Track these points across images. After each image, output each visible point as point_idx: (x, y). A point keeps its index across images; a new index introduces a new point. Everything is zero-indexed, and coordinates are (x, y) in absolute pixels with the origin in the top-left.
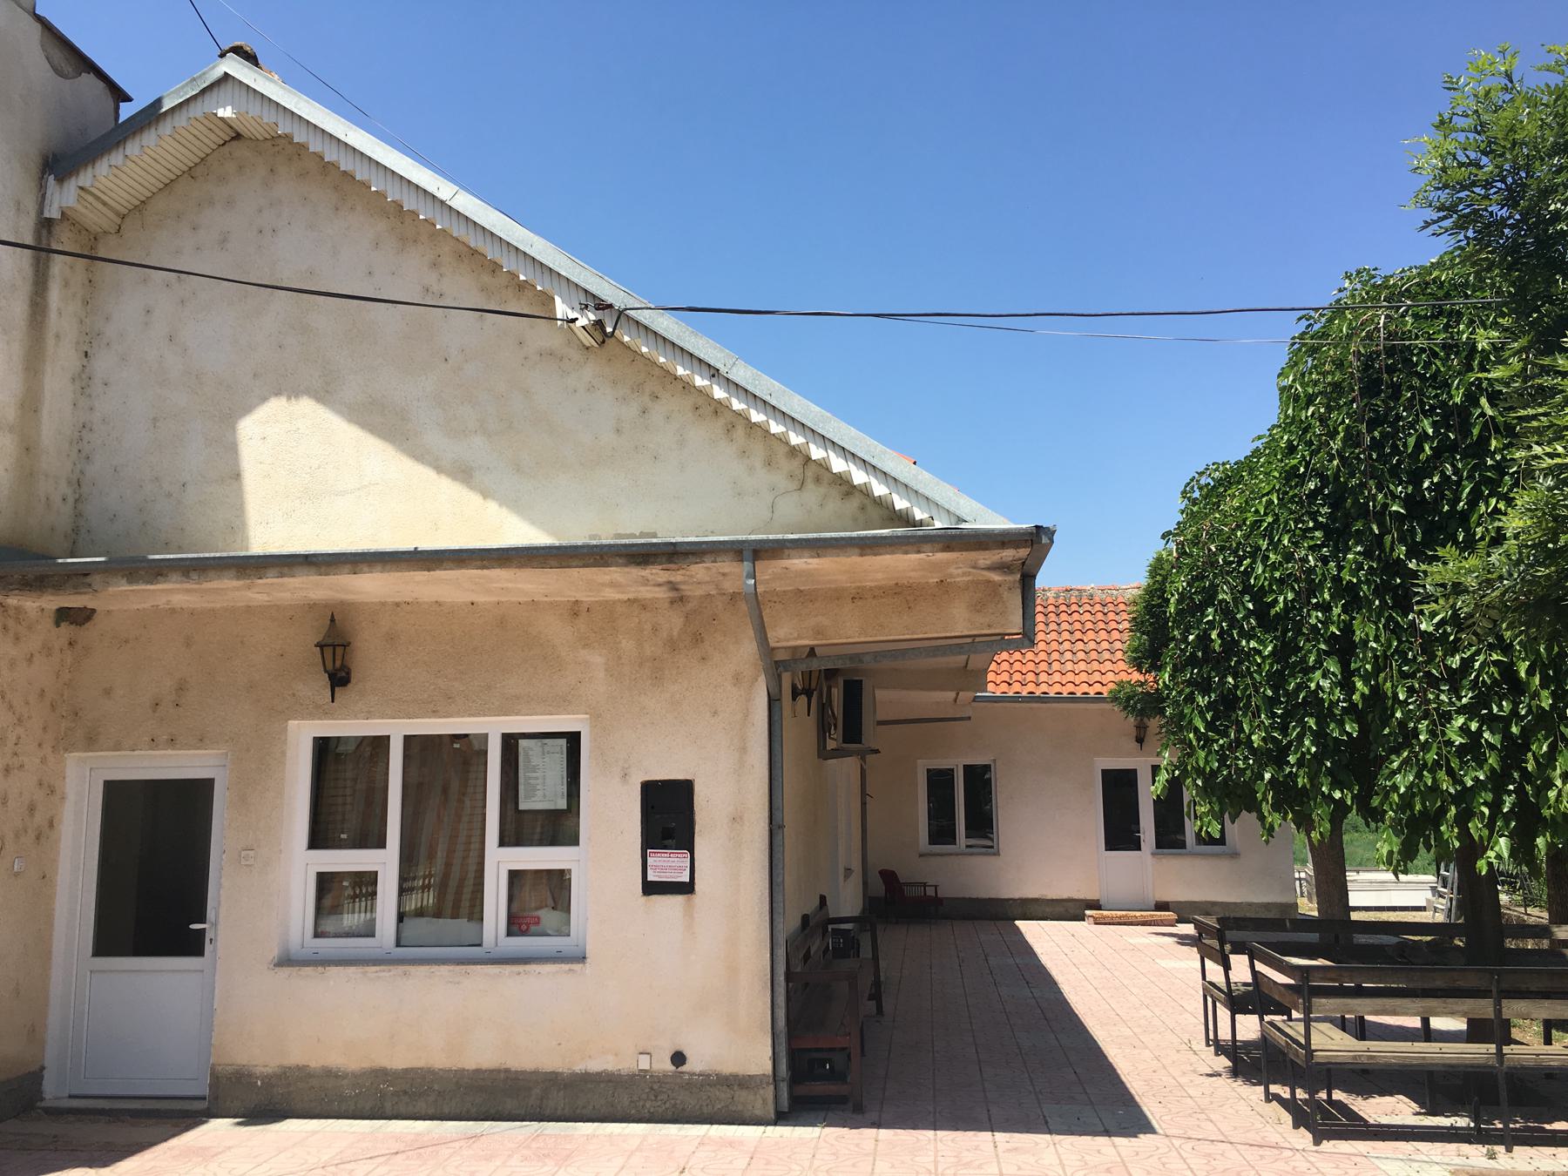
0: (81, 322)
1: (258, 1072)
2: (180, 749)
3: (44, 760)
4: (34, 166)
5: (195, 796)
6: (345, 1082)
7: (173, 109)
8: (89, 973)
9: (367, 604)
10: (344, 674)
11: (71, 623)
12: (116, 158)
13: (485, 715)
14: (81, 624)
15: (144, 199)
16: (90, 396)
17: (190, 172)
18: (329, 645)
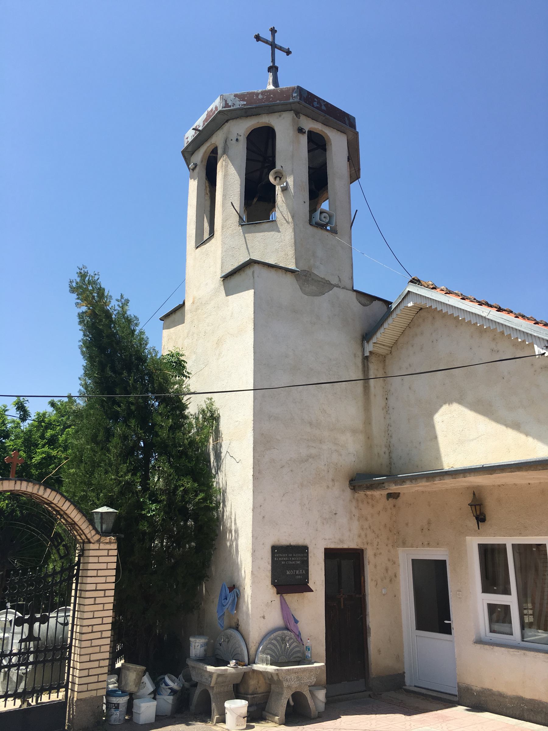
0: (383, 388)
1: (474, 689)
2: (431, 548)
3: (389, 551)
4: (359, 341)
5: (441, 565)
6: (507, 700)
7: (395, 308)
8: (415, 636)
9: (488, 486)
10: (483, 517)
11: (394, 498)
12: (382, 330)
13: (541, 536)
14: (396, 498)
15: (396, 339)
16: (389, 414)
17: (409, 326)
18: (473, 505)
